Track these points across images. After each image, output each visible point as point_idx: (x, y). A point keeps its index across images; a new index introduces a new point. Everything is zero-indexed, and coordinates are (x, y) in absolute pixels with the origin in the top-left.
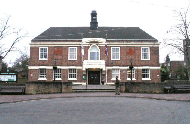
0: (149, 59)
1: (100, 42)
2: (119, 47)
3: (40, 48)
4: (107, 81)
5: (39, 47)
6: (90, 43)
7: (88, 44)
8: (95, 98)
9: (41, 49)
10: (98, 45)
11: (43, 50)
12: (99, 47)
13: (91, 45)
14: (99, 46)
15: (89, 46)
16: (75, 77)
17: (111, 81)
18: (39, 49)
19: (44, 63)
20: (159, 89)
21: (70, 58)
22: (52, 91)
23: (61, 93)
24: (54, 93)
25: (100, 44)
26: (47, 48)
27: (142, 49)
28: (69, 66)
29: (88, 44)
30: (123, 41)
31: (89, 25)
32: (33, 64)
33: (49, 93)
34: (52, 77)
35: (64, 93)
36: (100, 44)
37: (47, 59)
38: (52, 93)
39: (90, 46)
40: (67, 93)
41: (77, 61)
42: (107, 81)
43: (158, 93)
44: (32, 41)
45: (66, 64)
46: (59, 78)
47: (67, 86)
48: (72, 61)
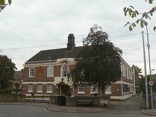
1: (69, 62)
2: (34, 67)
3: (30, 68)
4: (74, 94)
5: (29, 67)
6: (62, 62)
7: (61, 64)
8: (17, 105)
9: (49, 68)
11: (32, 70)
13: (63, 64)
15: (61, 65)
17: (78, 95)
18: (29, 69)
19: (51, 80)
20: (68, 102)
21: (30, 76)
22: (11, 100)
23: (17, 102)
24: (13, 102)
26: (34, 68)
28: (47, 81)
29: (61, 64)
30: (40, 63)
31: (66, 46)
33: (9, 101)
34: (27, 90)
35: (19, 102)
37: (34, 77)
38: (11, 102)
40: (21, 102)
42: (74, 94)
43: (103, 107)
44: (26, 63)
45: (46, 80)
46: (50, 91)
47: (21, 97)
48: (50, 78)
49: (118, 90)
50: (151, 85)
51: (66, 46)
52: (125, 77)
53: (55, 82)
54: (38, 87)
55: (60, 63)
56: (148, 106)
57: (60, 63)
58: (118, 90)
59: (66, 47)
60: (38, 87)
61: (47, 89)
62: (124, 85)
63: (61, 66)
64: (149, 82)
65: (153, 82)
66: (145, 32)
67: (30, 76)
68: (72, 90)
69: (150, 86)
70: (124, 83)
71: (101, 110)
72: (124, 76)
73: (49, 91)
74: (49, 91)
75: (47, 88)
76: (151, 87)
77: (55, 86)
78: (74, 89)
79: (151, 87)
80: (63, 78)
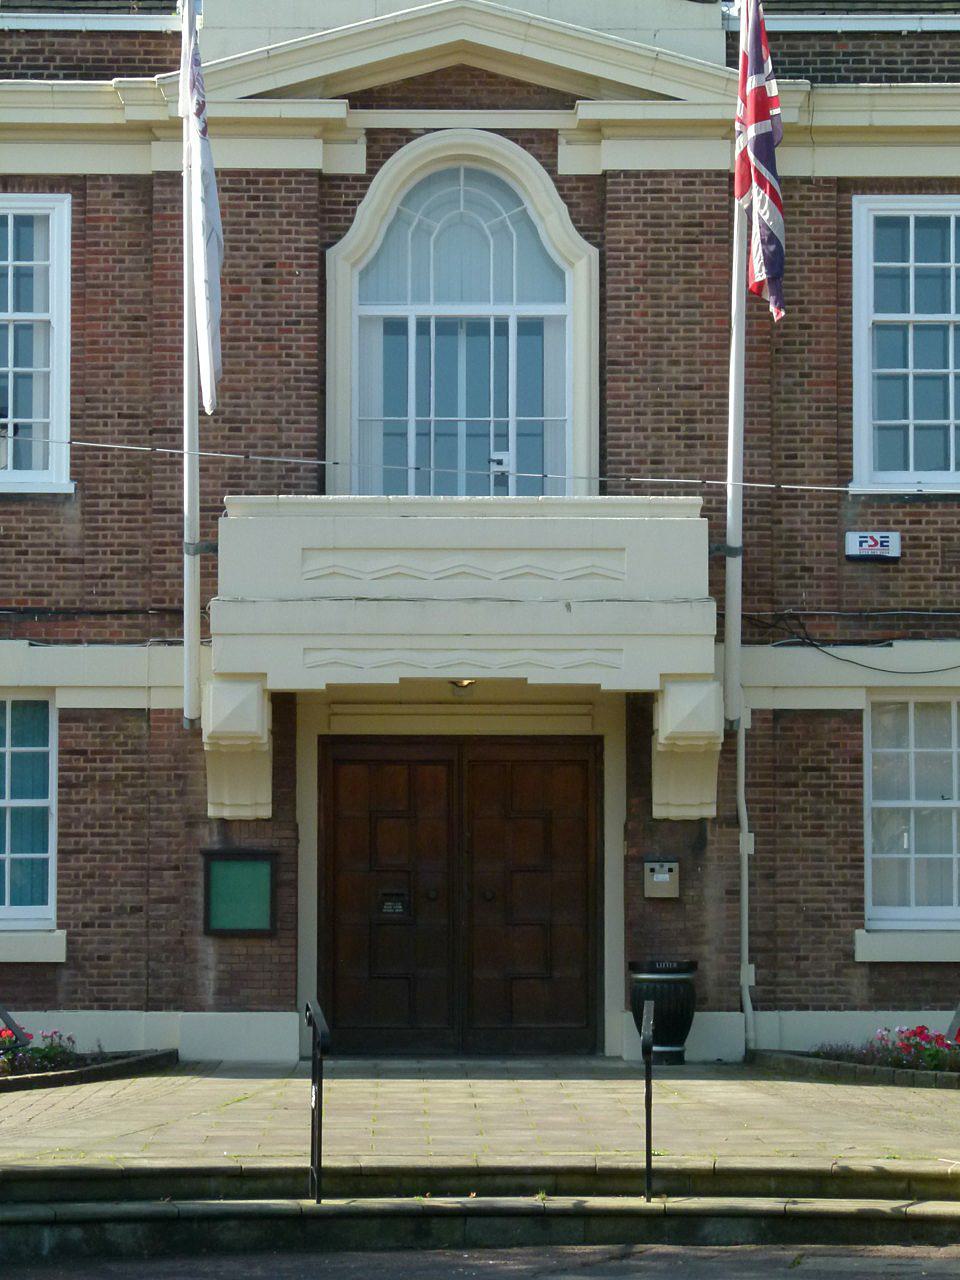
0: (54, 476)
3: (865, 210)
9: (886, 225)
10: (542, 145)
12: (566, 186)
14: (574, 160)
16: (30, 892)
25: (596, 131)
27: (886, 225)
32: (125, 620)
36: (596, 131)
39: (375, 162)
41: (70, 526)
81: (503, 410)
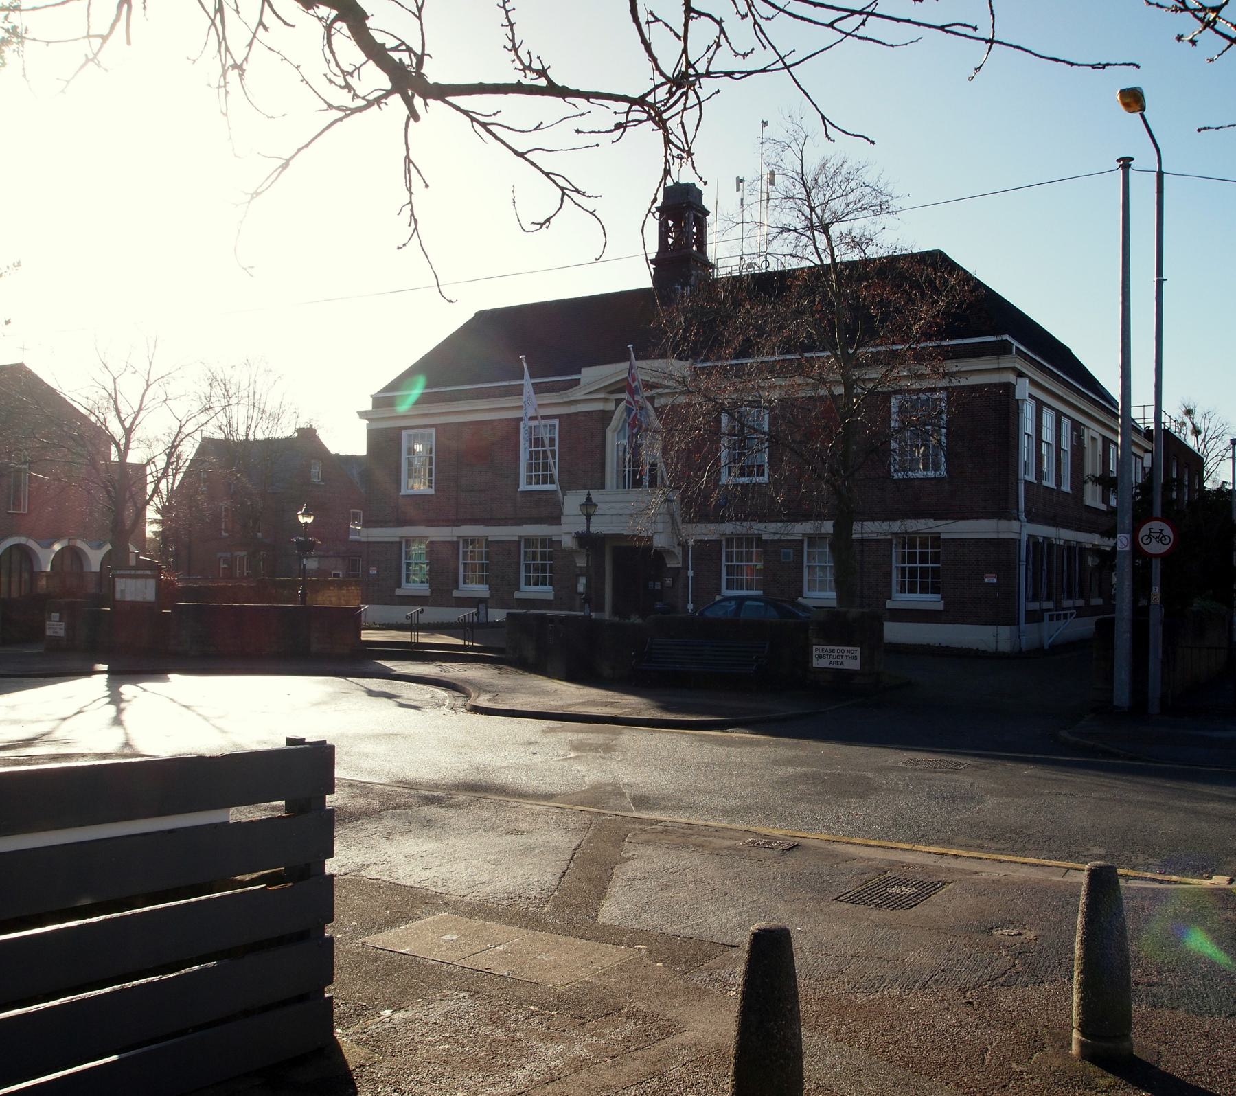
12: (656, 409)
14: (658, 403)
15: (611, 406)
25: (661, 395)
28: (519, 522)
29: (606, 400)
31: (640, 278)
46: (540, 588)
47: (997, 649)
49: (991, 579)
50: (1155, 548)
51: (640, 278)
52: (1066, 488)
53: (565, 528)
54: (729, 559)
55: (602, 395)
56: (1122, 695)
57: (602, 395)
58: (991, 579)
59: (648, 283)
60: (461, 561)
61: (523, 574)
62: (1033, 541)
63: (606, 417)
64: (1144, 530)
65: (1168, 531)
66: (1144, 159)
67: (763, 475)
68: (1030, 595)
69: (1148, 557)
70: (1043, 531)
71: (573, 709)
72: (1050, 483)
73: (912, 591)
74: (533, 588)
75: (523, 569)
76: (1157, 567)
77: (570, 554)
78: (690, 573)
79: (1157, 567)
80: (589, 499)
81: (629, 471)
